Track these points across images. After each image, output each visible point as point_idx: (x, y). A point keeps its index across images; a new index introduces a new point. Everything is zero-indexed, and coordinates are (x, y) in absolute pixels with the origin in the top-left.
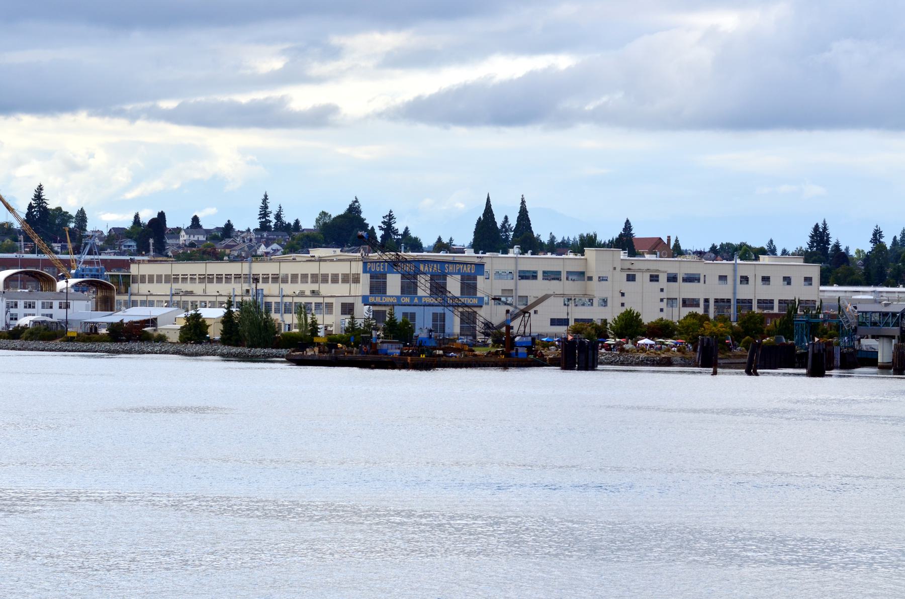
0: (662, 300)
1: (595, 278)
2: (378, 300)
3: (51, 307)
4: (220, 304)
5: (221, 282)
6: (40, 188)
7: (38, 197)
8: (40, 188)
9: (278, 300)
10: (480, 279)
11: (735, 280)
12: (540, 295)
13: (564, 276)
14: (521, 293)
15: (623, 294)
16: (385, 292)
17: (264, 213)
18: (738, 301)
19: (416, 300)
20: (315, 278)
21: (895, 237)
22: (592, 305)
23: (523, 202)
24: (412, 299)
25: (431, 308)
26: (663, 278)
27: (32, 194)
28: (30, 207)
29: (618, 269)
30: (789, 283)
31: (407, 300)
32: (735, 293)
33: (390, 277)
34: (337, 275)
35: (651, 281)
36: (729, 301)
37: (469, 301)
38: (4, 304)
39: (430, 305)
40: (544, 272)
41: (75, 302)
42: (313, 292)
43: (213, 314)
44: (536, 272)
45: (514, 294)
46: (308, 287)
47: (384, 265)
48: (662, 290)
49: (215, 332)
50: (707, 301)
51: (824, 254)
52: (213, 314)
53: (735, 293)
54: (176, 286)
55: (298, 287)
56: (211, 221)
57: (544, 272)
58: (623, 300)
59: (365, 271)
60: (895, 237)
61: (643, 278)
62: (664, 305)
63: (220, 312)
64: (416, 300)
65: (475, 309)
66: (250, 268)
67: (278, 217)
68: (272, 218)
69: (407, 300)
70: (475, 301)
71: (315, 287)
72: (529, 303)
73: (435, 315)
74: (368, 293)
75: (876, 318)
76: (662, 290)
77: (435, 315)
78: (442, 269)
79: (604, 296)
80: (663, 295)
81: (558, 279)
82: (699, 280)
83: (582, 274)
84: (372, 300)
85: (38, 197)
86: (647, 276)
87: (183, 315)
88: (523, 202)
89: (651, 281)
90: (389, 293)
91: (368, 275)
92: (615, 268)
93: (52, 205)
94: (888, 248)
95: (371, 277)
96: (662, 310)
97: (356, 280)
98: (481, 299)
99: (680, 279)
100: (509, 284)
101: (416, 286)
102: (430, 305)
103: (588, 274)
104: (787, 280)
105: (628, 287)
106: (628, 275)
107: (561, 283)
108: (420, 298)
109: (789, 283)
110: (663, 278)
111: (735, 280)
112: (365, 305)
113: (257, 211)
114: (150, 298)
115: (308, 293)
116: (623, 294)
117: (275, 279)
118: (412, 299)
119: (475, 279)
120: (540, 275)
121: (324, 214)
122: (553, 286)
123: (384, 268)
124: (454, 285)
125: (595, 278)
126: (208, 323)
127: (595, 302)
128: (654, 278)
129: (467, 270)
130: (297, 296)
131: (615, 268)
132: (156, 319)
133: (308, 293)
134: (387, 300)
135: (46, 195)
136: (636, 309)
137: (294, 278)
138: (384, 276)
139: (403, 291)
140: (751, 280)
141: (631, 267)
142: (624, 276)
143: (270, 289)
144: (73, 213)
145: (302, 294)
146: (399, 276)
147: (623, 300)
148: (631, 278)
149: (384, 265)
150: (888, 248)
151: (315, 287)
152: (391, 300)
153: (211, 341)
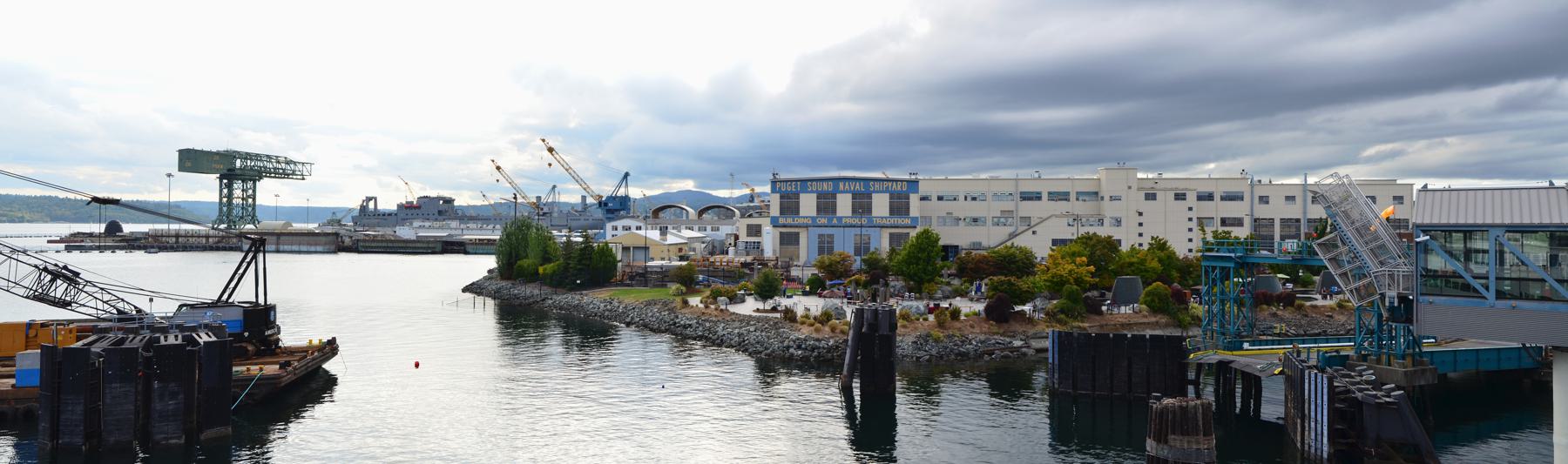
1: (1107, 198)
2: (790, 221)
11: (1305, 201)
13: (1073, 197)
18: (1309, 221)
24: (830, 220)
26: (1191, 198)
29: (1135, 187)
30: (1395, 198)
31: (824, 221)
32: (1305, 213)
35: (182, 168)
36: (1298, 220)
51: (65, 268)
53: (1305, 213)
58: (1141, 219)
69: (824, 221)
70: (907, 221)
82: (1242, 199)
83: (1096, 193)
84: (782, 221)
89: (182, 168)
90: (802, 213)
95: (782, 197)
99: (1217, 197)
100: (1009, 206)
106: (749, 226)
110: (1191, 198)
111: (1305, 201)
118: (830, 220)
120: (1045, 196)
122: (1062, 206)
124: (844, 205)
125: (1107, 198)
127: (1106, 222)
128: (1180, 197)
129: (897, 187)
134: (800, 221)
136: (339, 391)
139: (819, 210)
142: (1142, 194)
146: (887, 196)
148: (1151, 197)
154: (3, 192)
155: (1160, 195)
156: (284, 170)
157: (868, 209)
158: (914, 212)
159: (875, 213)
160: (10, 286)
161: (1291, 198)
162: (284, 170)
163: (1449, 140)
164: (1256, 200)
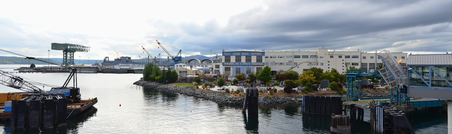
1: (319, 57)
2: (228, 64)
11: (376, 58)
13: (309, 57)
18: (377, 64)
21: (82, 49)
24: (239, 63)
26: (343, 57)
29: (327, 54)
30: (402, 57)
31: (237, 64)
32: (376, 61)
35: (52, 49)
36: (374, 64)
53: (376, 61)
58: (329, 63)
60: (82, 49)
69: (237, 64)
70: (262, 64)
82: (358, 57)
83: (316, 56)
84: (225, 64)
89: (52, 49)
90: (231, 62)
94: (94, 106)
95: (225, 57)
99: (351, 57)
100: (291, 59)
106: (216, 65)
110: (343, 57)
111: (376, 58)
118: (239, 63)
120: (301, 57)
122: (306, 60)
124: (243, 59)
125: (319, 57)
127: (319, 64)
128: (340, 57)
129: (259, 54)
134: (231, 64)
136: (98, 113)
139: (236, 61)
142: (329, 56)
146: (256, 57)
148: (332, 57)
150: (94, 106)
155: (334, 56)
157: (250, 60)
158: (263, 61)
159: (252, 62)
161: (372, 57)
163: (418, 40)
164: (362, 58)
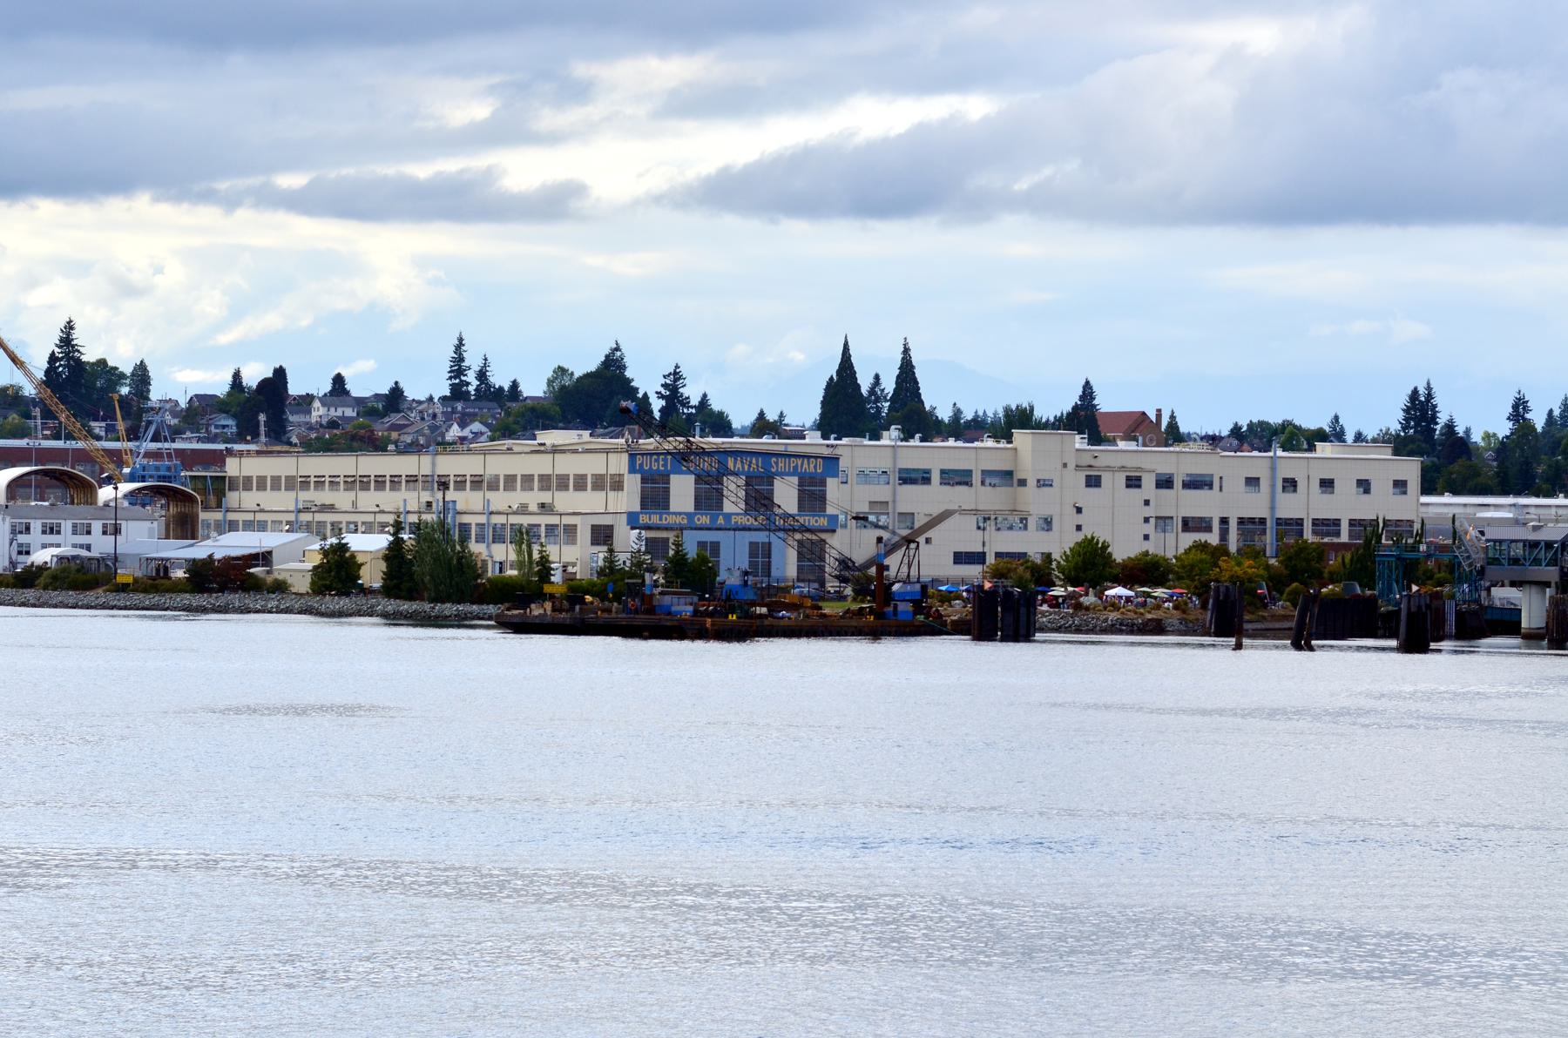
0: (1146, 520)
1: (1032, 482)
2: (655, 519)
3: (89, 533)
4: (382, 527)
5: (383, 489)
6: (70, 326)
7: (66, 341)
8: (70, 326)
9: (482, 519)
10: (832, 483)
11: (1273, 486)
12: (936, 511)
13: (977, 478)
14: (902, 508)
15: (1079, 510)
16: (667, 507)
17: (458, 369)
18: (1279, 522)
19: (721, 521)
20: (546, 482)
22: (1026, 528)
23: (906, 351)
24: (714, 519)
25: (747, 533)
26: (1149, 482)
27: (56, 337)
28: (53, 358)
29: (1071, 466)
30: (1367, 491)
31: (705, 520)
32: (1273, 508)
33: (675, 480)
34: (583, 477)
35: (1128, 486)
36: (1263, 521)
37: (813, 522)
38: (7, 527)
39: (745, 529)
40: (943, 472)
41: (131, 523)
42: (543, 506)
43: (368, 545)
44: (928, 472)
45: (890, 510)
46: (534, 498)
47: (665, 460)
48: (1147, 503)
49: (372, 575)
50: (1224, 521)
52: (368, 545)
53: (1273, 508)
54: (304, 496)
55: (516, 498)
56: (366, 382)
57: (943, 472)
58: (1080, 519)
59: (632, 470)
61: (1114, 482)
62: (1150, 528)
63: (381, 541)
64: (721, 521)
65: (823, 536)
66: (434, 464)
67: (482, 375)
68: (471, 377)
69: (705, 520)
70: (823, 522)
71: (546, 497)
72: (917, 525)
73: (753, 546)
74: (637, 508)
75: (1518, 551)
76: (1147, 503)
77: (753, 546)
78: (766, 466)
79: (1046, 512)
80: (1149, 512)
81: (966, 484)
82: (1210, 486)
83: (1009, 474)
84: (644, 519)
85: (66, 341)
86: (1121, 479)
87: (317, 547)
88: (906, 351)
89: (1128, 486)
90: (673, 507)
91: (638, 477)
92: (1065, 465)
93: (89, 355)
94: (1539, 430)
95: (644, 481)
96: (1146, 537)
97: (617, 485)
98: (834, 518)
99: (1178, 483)
100: (882, 492)
101: (720, 495)
102: (745, 529)
103: (1019, 475)
104: (1364, 485)
105: (1088, 497)
107: (972, 490)
108: (728, 516)
109: (1367, 491)
110: (1149, 482)
111: (1273, 486)
112: (633, 528)
113: (446, 366)
114: (260, 517)
115: (533, 507)
116: (1079, 510)
117: (477, 483)
118: (714, 519)
119: (823, 483)
120: (936, 477)
121: (561, 371)
122: (958, 496)
123: (665, 465)
124: (786, 495)
125: (1032, 482)
126: (360, 559)
127: (1032, 523)
128: (1133, 482)
129: (809, 467)
130: (515, 513)
131: (1065, 465)
132: (270, 553)
133: (533, 507)
134: (671, 520)
135: (79, 337)
136: (1102, 536)
137: (510, 481)
138: (665, 478)
139: (698, 505)
140: (1301, 486)
141: (1093, 462)
142: (1081, 477)
143: (467, 501)
144: (127, 369)
145: (523, 510)
146: (692, 478)
147: (1080, 519)
148: (1093, 482)
149: (665, 460)
150: (1539, 430)
151: (546, 497)
152: (678, 520)
153: (365, 591)
154: (1561, 500)
156: (1551, 411)
160: (1566, 981)
162: (1551, 411)
